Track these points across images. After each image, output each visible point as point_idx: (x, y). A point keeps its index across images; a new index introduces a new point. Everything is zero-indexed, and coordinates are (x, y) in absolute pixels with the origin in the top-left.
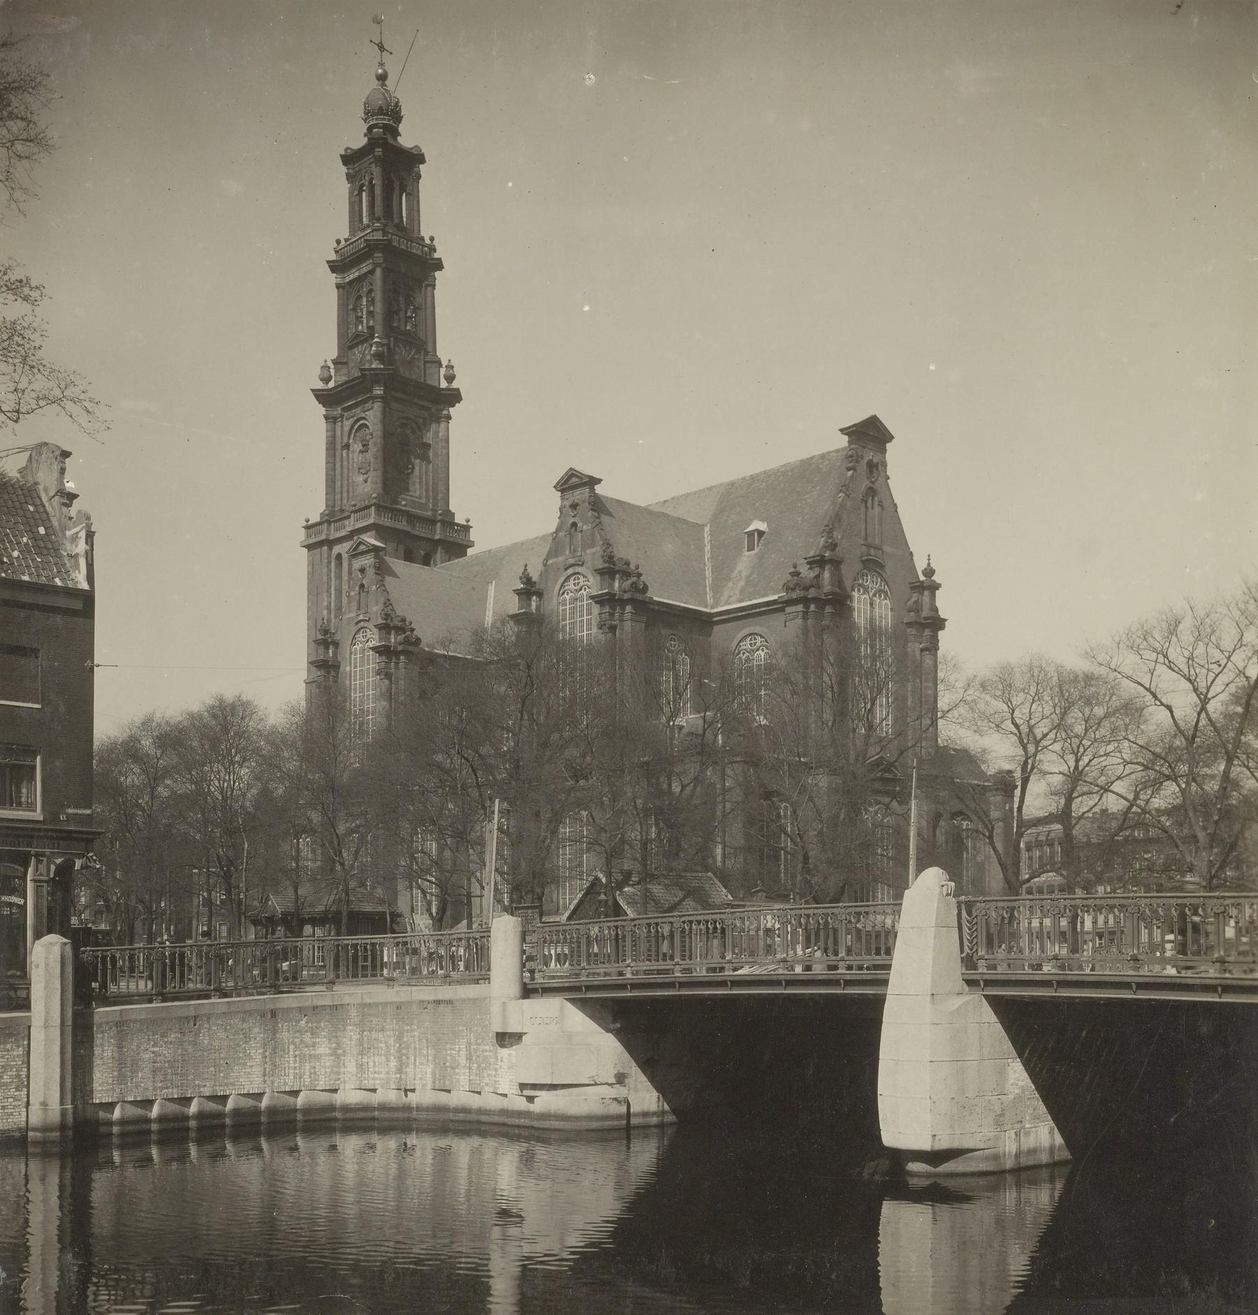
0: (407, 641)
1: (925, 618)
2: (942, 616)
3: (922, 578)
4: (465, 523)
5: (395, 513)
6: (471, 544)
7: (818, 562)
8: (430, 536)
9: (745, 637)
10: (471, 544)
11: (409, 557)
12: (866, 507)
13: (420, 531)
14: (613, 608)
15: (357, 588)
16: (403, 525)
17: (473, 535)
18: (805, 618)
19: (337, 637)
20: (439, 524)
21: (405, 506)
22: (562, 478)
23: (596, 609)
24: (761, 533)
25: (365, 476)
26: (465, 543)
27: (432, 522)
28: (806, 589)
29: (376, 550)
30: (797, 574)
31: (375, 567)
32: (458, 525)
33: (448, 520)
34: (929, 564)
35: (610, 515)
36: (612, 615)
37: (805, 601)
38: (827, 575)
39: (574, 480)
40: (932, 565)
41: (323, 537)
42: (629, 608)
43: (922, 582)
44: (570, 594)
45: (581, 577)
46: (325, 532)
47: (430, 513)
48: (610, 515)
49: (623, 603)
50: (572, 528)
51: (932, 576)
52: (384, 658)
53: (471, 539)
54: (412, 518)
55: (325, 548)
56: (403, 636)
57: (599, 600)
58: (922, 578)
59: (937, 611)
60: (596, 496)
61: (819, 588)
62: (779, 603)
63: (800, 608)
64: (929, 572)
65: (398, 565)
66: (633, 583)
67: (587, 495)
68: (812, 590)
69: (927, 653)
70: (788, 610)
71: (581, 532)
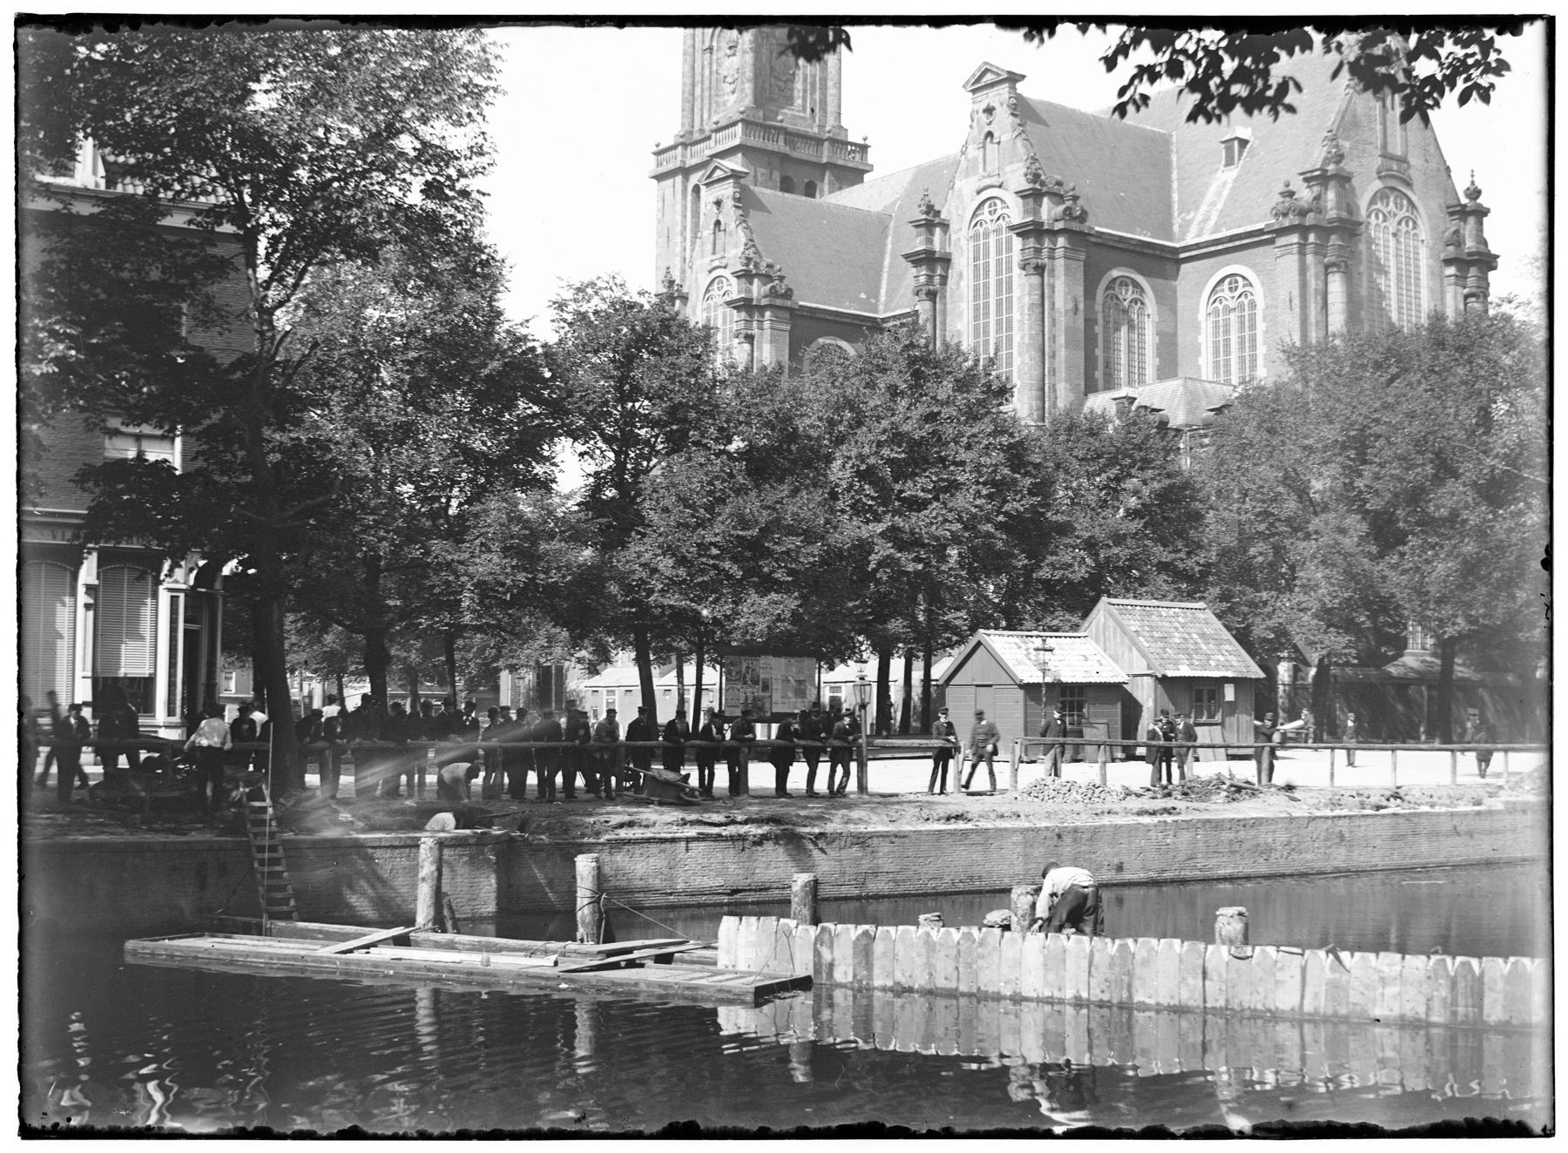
0: (773, 293)
1: (1470, 254)
2: (1494, 251)
3: (1464, 200)
4: (862, 142)
5: (768, 130)
6: (870, 169)
7: (1320, 178)
8: (814, 159)
9: (1222, 281)
10: (870, 169)
11: (787, 186)
12: (1384, 106)
13: (804, 152)
14: (1039, 241)
15: (712, 226)
16: (780, 146)
17: (872, 157)
18: (1302, 254)
19: (685, 290)
20: (826, 144)
21: (781, 121)
22: (974, 75)
23: (1017, 243)
24: (1243, 143)
25: (733, 86)
26: (861, 167)
27: (819, 142)
28: (1303, 213)
29: (735, 175)
30: (1291, 194)
31: (734, 199)
32: (852, 144)
33: (839, 143)
34: (1473, 183)
35: (850, 48)
36: (1038, 251)
37: (1303, 230)
38: (1331, 195)
39: (989, 78)
40: (1477, 184)
41: (678, 164)
42: (1061, 241)
43: (1465, 206)
44: (1224, 302)
45: (998, 202)
46: (679, 158)
47: (816, 130)
48: (850, 48)
49: (1054, 234)
50: (986, 138)
51: (1478, 197)
52: (743, 315)
53: (870, 161)
54: (792, 137)
55: (679, 179)
56: (769, 286)
57: (1023, 231)
58: (1464, 200)
59: (1486, 244)
60: (1019, 97)
61: (1320, 212)
62: (1269, 233)
63: (1295, 238)
64: (1474, 193)
65: (768, 194)
66: (1068, 209)
67: (1007, 96)
68: (1311, 215)
69: (1473, 299)
70: (1281, 241)
71: (999, 143)
